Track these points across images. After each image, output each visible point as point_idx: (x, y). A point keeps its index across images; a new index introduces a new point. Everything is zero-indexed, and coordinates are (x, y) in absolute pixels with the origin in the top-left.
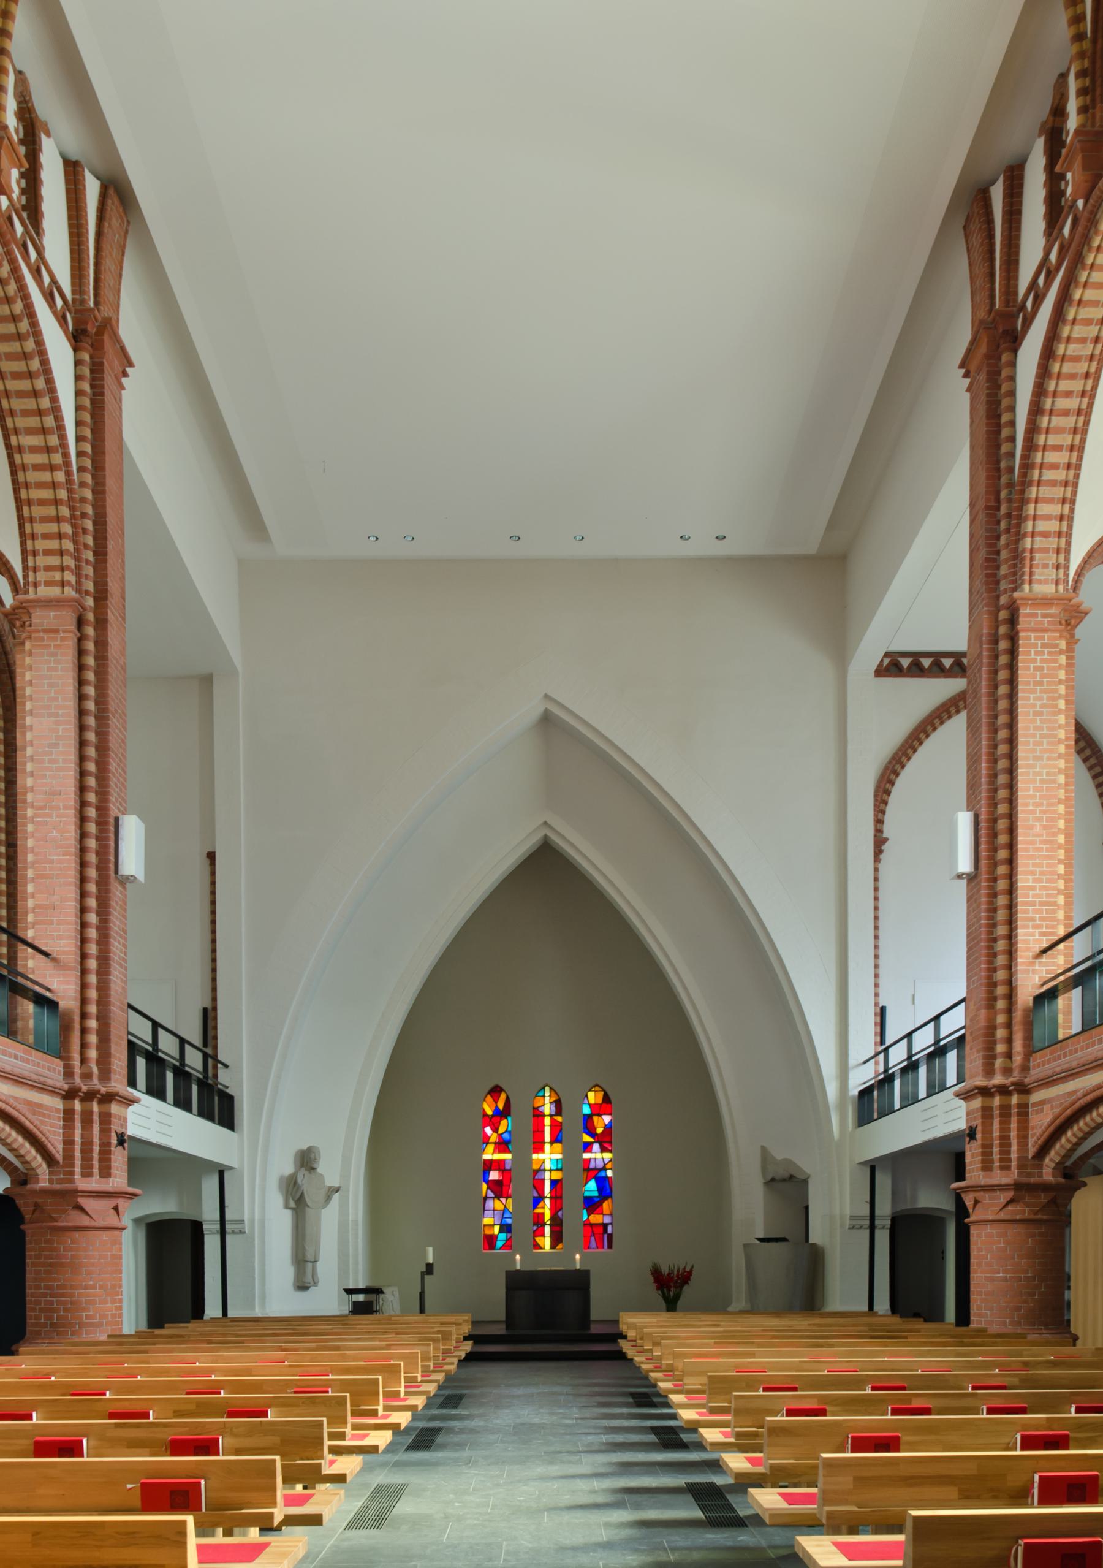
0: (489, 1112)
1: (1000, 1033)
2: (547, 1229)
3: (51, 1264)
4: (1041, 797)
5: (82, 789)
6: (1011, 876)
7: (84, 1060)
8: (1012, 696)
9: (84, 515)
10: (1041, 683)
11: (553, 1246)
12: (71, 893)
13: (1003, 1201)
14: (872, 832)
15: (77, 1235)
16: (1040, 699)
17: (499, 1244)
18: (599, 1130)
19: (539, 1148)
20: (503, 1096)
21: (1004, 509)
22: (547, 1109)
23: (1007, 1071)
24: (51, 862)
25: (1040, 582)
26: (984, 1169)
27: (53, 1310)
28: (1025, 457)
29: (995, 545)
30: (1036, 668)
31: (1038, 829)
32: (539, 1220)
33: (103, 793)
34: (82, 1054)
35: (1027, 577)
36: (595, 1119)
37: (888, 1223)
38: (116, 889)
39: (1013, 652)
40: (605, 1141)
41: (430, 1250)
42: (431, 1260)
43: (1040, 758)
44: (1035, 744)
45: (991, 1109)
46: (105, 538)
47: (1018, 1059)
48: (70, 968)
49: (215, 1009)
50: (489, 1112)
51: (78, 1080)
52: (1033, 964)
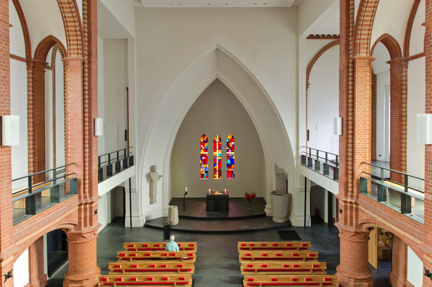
0: (202, 141)
1: (350, 185)
2: (217, 172)
3: (75, 254)
4: (362, 116)
5: (84, 112)
6: (353, 139)
7: (84, 193)
8: (353, 85)
9: (85, 32)
10: (362, 82)
11: (219, 177)
12: (81, 144)
13: (351, 235)
14: (306, 82)
15: (82, 244)
16: (362, 87)
17: (205, 176)
18: (231, 146)
19: (215, 151)
20: (206, 137)
21: (351, 29)
22: (217, 141)
23: (352, 197)
24: (75, 135)
25: (362, 53)
26: (345, 224)
27: (75, 267)
28: (358, 17)
29: (348, 39)
30: (361, 78)
31: (361, 126)
32: (215, 170)
33: (90, 113)
34: (84, 190)
35: (358, 51)
36: (230, 143)
37: (310, 190)
38: (94, 139)
39: (354, 72)
40: (232, 149)
41: (186, 188)
42: (186, 191)
43: (362, 105)
44: (361, 100)
45: (347, 206)
46: (91, 38)
47: (355, 194)
48: (81, 167)
49: (128, 130)
50: (202, 141)
51: (83, 199)
52: (360, 166)
